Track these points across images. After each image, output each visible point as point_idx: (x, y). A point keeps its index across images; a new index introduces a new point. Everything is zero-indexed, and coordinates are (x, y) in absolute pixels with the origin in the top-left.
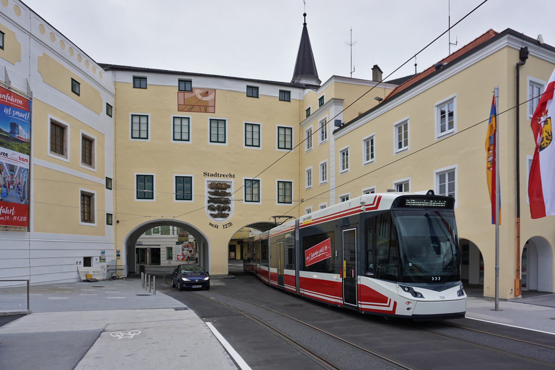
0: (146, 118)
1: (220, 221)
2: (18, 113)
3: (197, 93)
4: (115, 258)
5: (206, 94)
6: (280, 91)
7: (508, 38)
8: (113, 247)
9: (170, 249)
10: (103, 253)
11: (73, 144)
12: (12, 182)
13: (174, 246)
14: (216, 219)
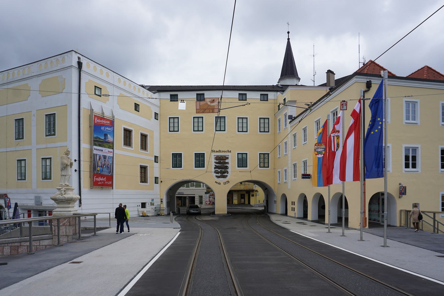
0: (177, 119)
1: (222, 180)
2: (107, 128)
3: (207, 100)
4: (159, 203)
5: (213, 101)
6: (261, 94)
7: (356, 77)
8: (159, 197)
9: (201, 197)
10: (153, 200)
11: (136, 139)
12: (105, 164)
13: (204, 195)
14: (220, 179)
